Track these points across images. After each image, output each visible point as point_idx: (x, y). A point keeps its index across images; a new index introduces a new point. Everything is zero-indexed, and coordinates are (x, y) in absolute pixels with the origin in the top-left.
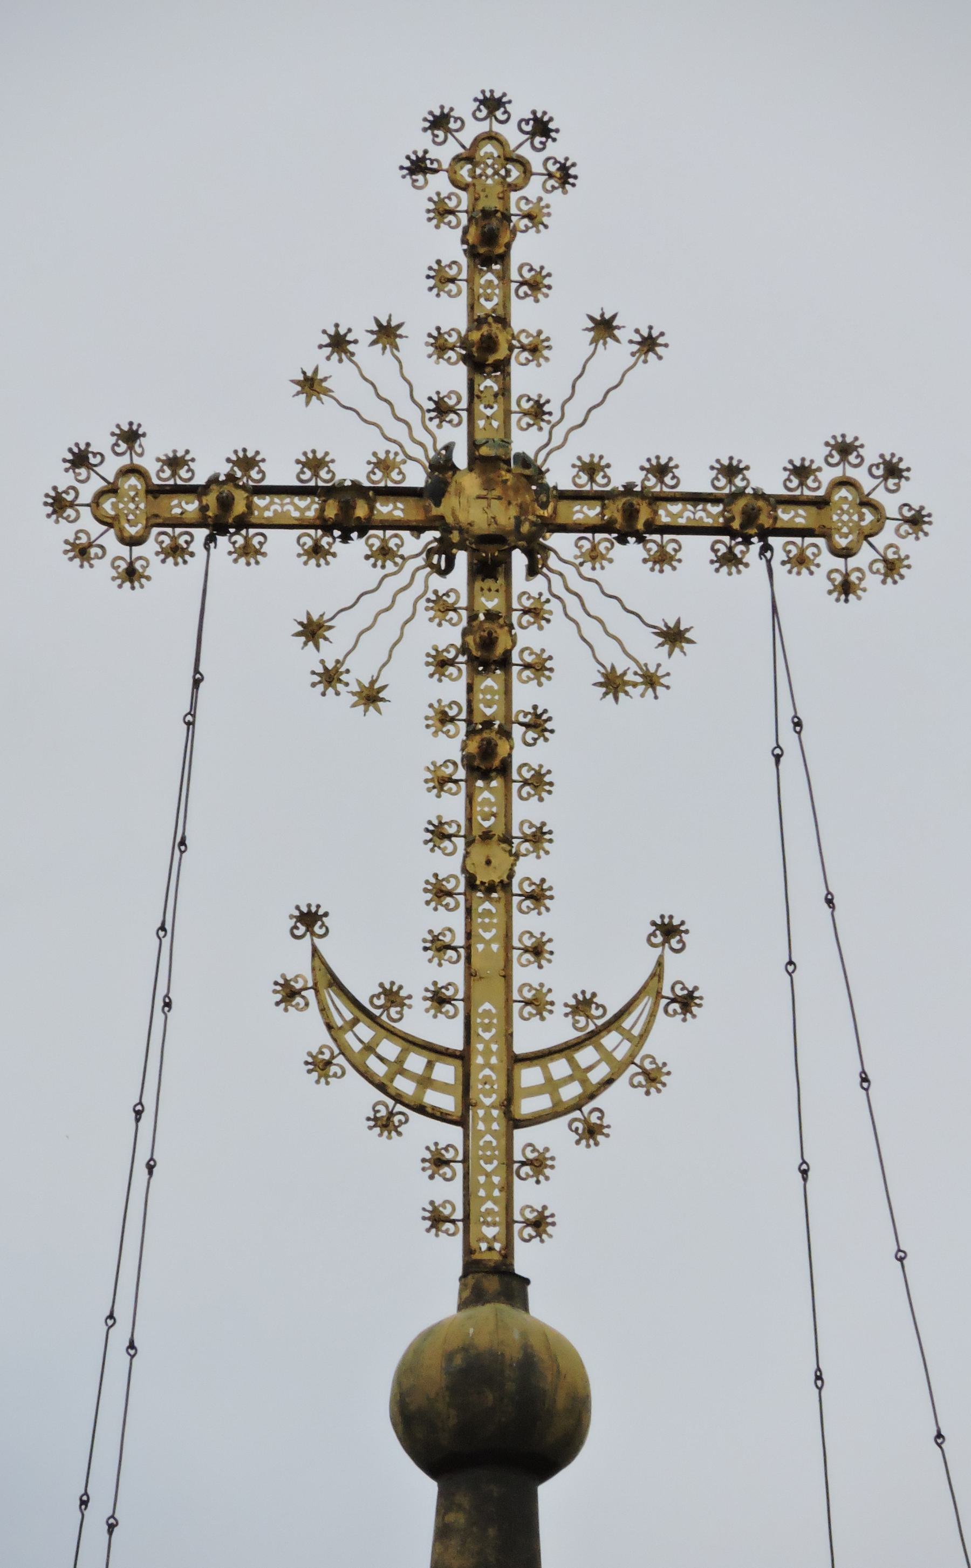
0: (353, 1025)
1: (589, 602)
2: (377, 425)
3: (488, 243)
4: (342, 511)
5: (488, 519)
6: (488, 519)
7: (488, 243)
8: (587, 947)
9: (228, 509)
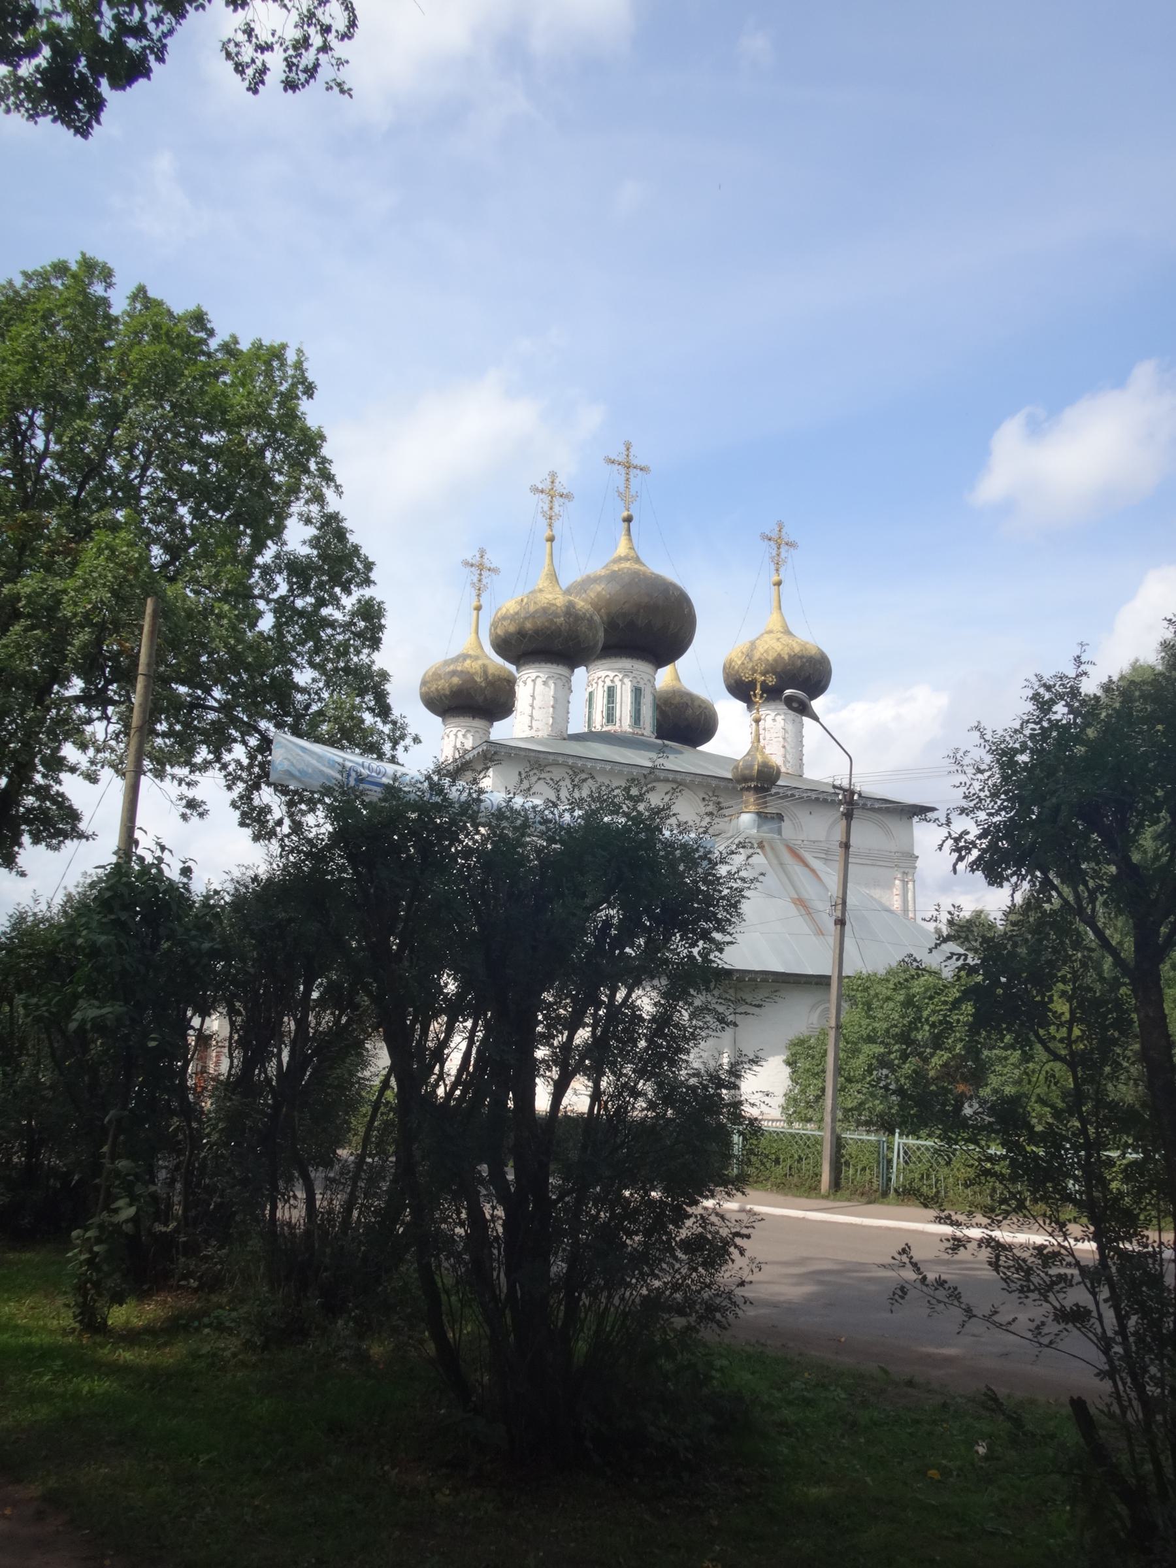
0: (620, 494)
1: (623, 471)
2: (633, 472)
5: (628, 466)
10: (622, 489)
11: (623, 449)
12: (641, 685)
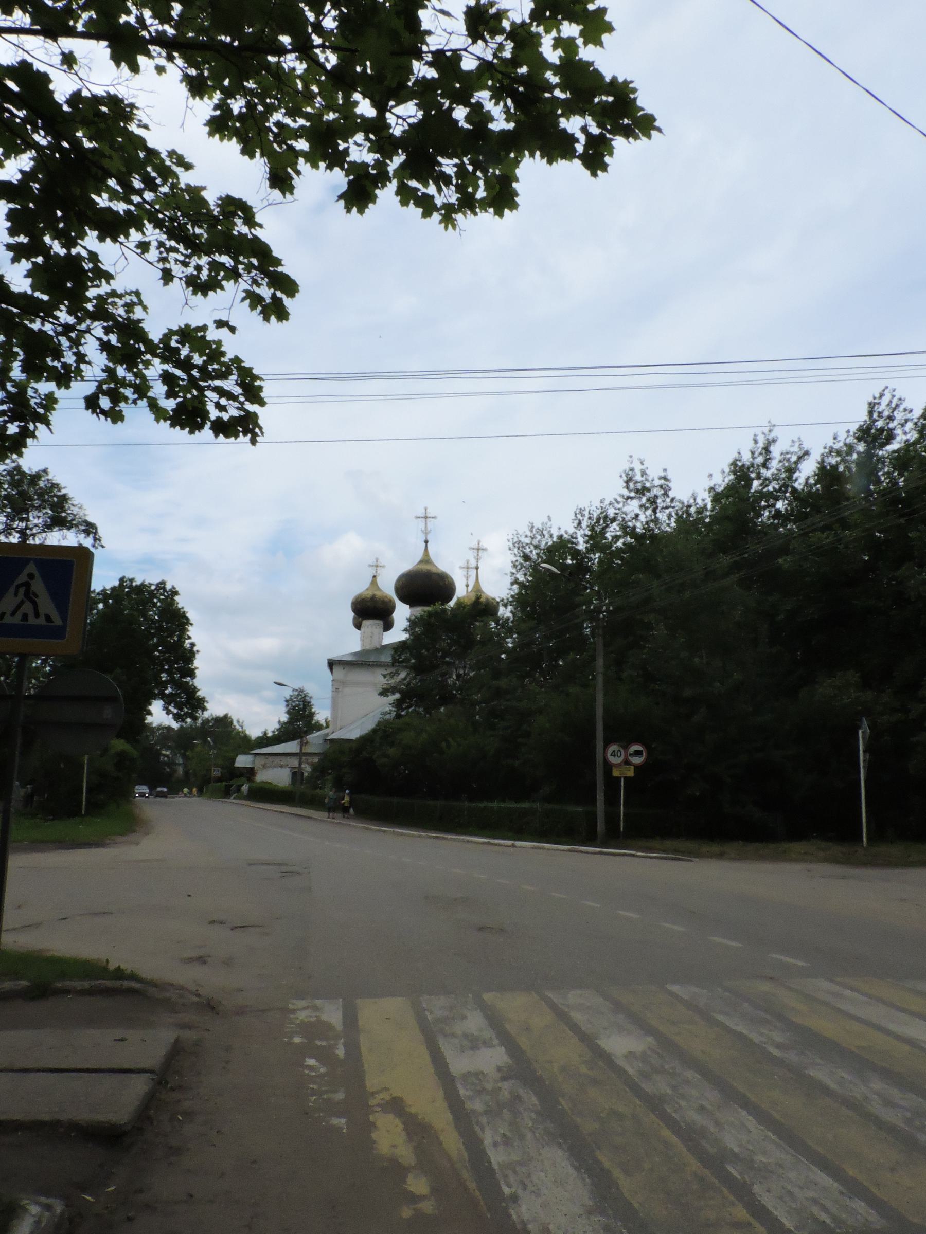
6: (426, 518)
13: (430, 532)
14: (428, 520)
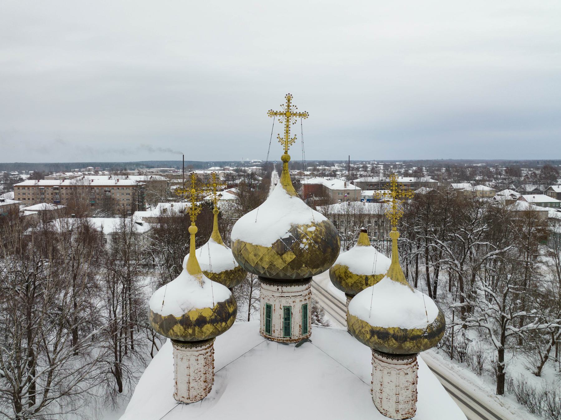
1: (283, 118)
3: (289, 101)
4: (288, 121)
7: (289, 101)
8: (292, 136)
9: (276, 114)
10: (282, 135)
11: (301, 110)
12: (271, 303)
13: (293, 140)
14: (293, 119)
